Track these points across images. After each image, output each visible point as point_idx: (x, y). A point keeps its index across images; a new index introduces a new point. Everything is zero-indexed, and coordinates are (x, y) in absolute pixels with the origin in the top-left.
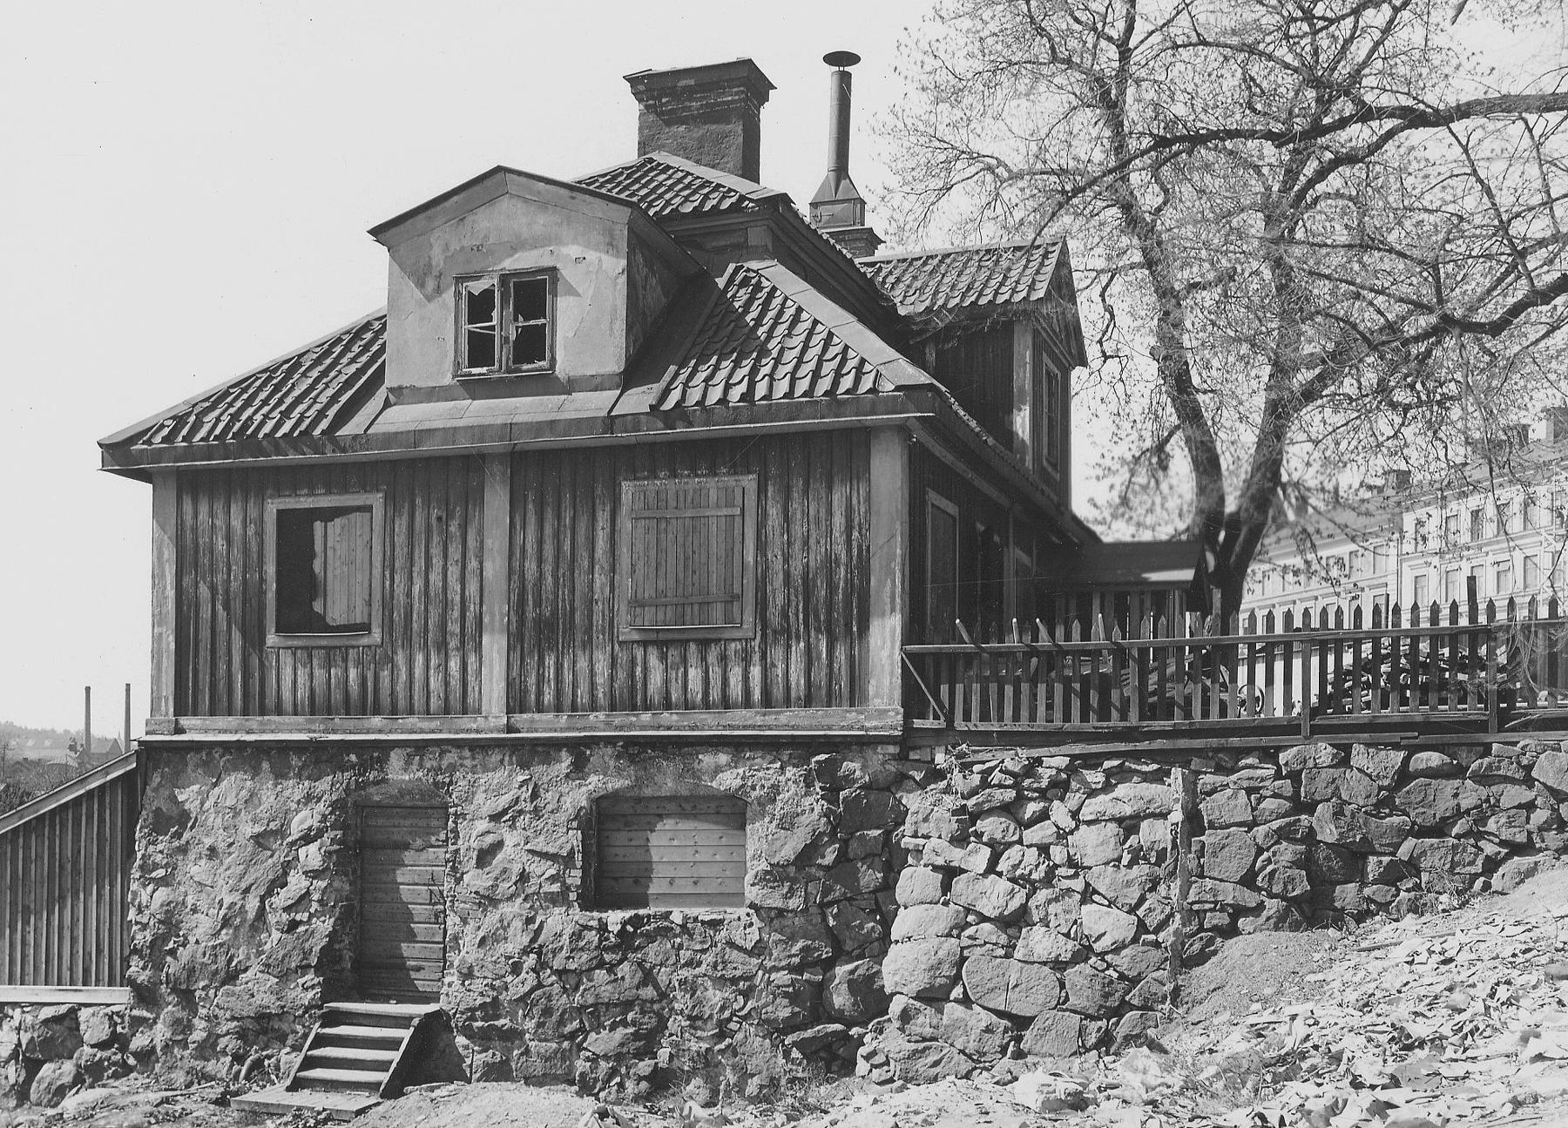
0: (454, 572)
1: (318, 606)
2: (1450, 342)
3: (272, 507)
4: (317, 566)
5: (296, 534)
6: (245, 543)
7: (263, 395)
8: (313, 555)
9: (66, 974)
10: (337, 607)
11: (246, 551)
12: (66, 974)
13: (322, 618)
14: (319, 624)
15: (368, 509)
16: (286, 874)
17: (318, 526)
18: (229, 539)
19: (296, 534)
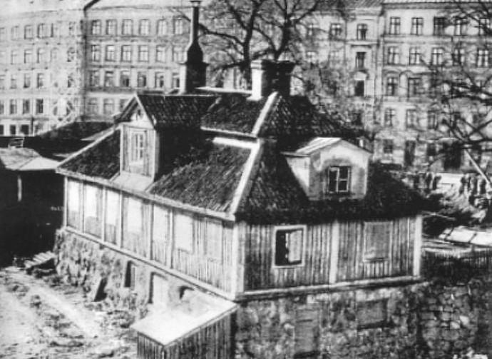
0: (323, 246)
1: (286, 256)
2: (232, 71)
3: (277, 228)
4: (287, 245)
5: (281, 236)
6: (266, 238)
7: (323, 234)
8: (285, 242)
9: (134, 157)
10: (292, 257)
11: (266, 241)
12: (134, 157)
13: (287, 260)
14: (287, 262)
15: (302, 230)
16: (130, 114)
17: (287, 235)
18: (261, 238)
19: (281, 236)
